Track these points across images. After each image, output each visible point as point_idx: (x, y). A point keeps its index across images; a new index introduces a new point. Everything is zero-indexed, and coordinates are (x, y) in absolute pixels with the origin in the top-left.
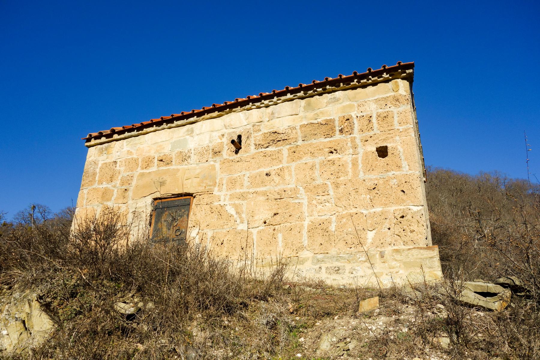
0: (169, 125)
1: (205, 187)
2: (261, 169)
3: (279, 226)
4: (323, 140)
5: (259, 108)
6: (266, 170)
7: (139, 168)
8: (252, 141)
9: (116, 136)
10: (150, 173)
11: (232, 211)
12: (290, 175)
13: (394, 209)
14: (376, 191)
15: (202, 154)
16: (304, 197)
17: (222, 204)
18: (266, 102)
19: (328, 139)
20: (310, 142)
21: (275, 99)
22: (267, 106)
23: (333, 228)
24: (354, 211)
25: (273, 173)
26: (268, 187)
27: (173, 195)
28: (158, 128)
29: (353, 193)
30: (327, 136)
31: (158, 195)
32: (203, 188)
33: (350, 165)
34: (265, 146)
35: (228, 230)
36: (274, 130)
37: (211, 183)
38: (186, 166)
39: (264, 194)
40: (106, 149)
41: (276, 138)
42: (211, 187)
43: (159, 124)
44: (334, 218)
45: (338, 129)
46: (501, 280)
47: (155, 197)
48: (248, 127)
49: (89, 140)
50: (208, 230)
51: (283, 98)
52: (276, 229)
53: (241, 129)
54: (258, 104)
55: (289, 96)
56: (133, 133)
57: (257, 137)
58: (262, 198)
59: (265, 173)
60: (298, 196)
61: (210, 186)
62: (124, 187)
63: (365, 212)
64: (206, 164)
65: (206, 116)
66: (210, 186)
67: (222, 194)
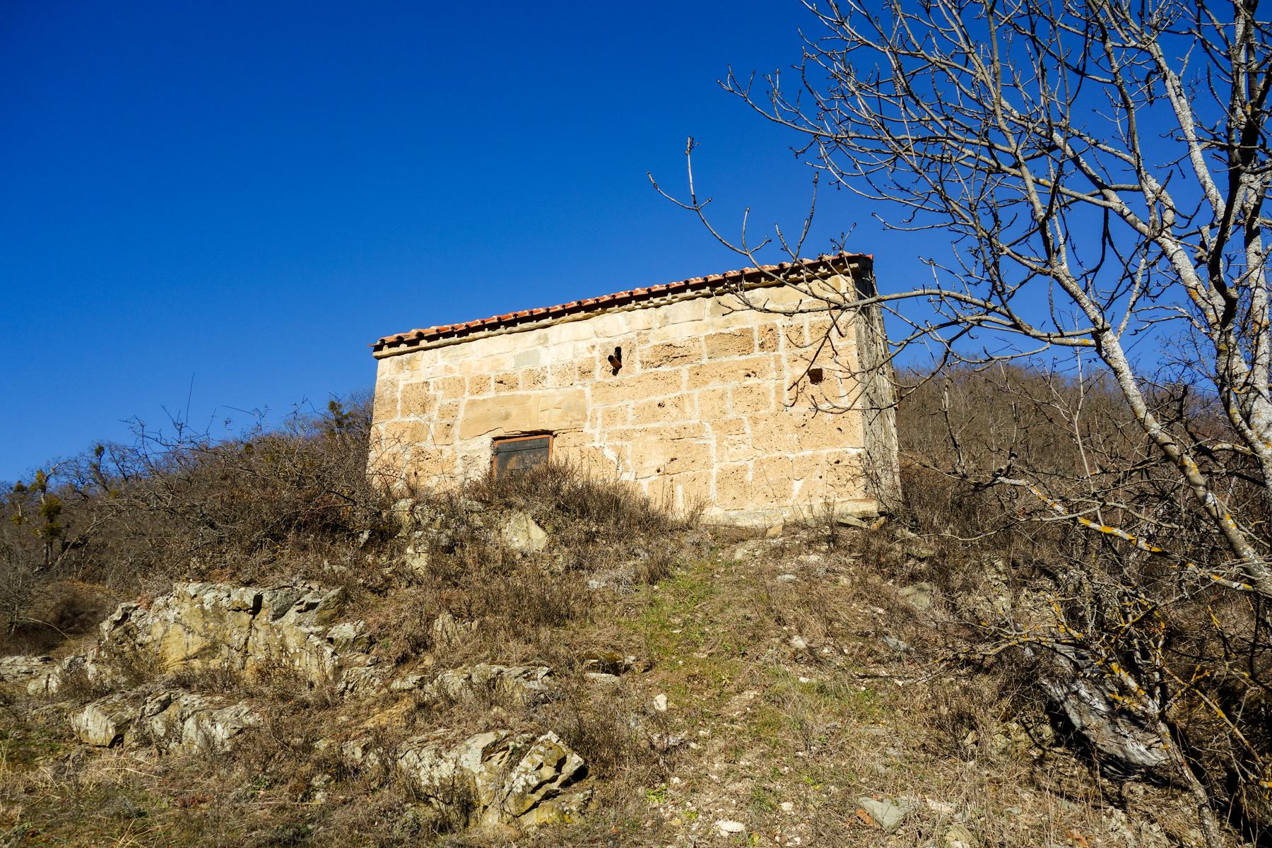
0: (509, 329)
2: (652, 398)
4: (736, 358)
5: (645, 308)
6: (659, 399)
7: (467, 394)
8: (637, 356)
9: (424, 343)
12: (692, 406)
13: (828, 452)
14: (805, 429)
15: (563, 374)
18: (657, 300)
19: (744, 357)
21: (669, 296)
22: (657, 306)
23: (749, 477)
24: (778, 454)
25: (668, 404)
28: (491, 333)
29: (776, 431)
30: (743, 352)
31: (500, 433)
33: (773, 394)
36: (669, 342)
39: (657, 432)
40: (409, 362)
41: (671, 354)
43: (493, 327)
44: (751, 464)
45: (757, 342)
48: (631, 336)
49: (379, 348)
51: (681, 295)
53: (620, 338)
54: (644, 303)
55: (689, 293)
56: (452, 339)
57: (643, 351)
58: (654, 438)
62: (445, 421)
63: (791, 456)
64: (571, 389)
65: (567, 317)
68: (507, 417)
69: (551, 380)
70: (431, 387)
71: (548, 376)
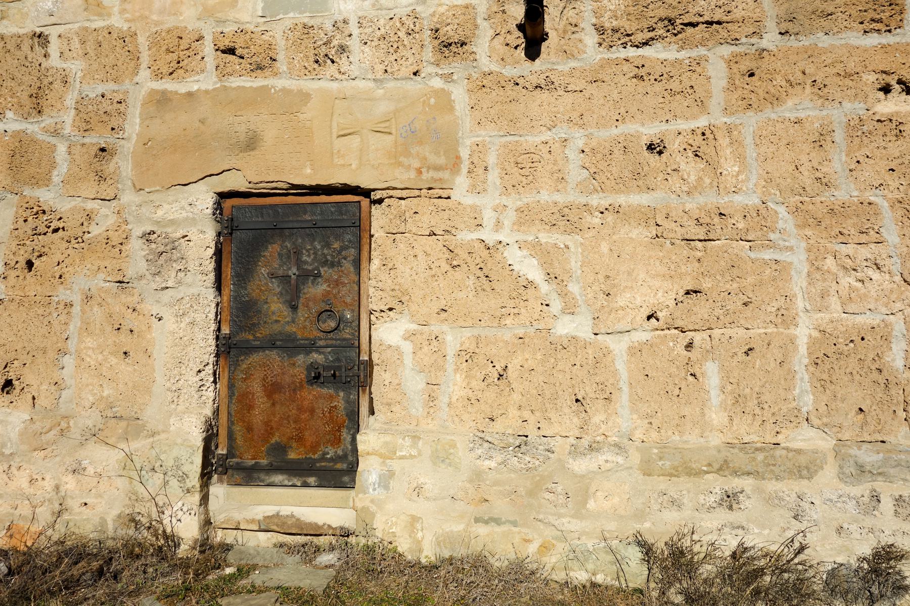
1: (419, 171)
2: (630, 128)
3: (705, 335)
6: (650, 131)
7: (144, 74)
10: (190, 94)
11: (531, 270)
16: (793, 242)
17: (491, 238)
20: (805, 42)
25: (674, 145)
26: (658, 194)
27: (294, 187)
32: (413, 174)
34: (640, 37)
35: (521, 332)
37: (442, 161)
38: (335, 85)
39: (647, 217)
42: (440, 175)
46: (237, 428)
47: (226, 189)
50: (445, 327)
52: (696, 343)
58: (640, 233)
59: (645, 141)
60: (772, 236)
61: (438, 168)
62: (95, 139)
64: (414, 86)
66: (438, 168)
67: (487, 203)
68: (251, 143)
69: (361, 57)
70: (54, 48)
71: (354, 44)
